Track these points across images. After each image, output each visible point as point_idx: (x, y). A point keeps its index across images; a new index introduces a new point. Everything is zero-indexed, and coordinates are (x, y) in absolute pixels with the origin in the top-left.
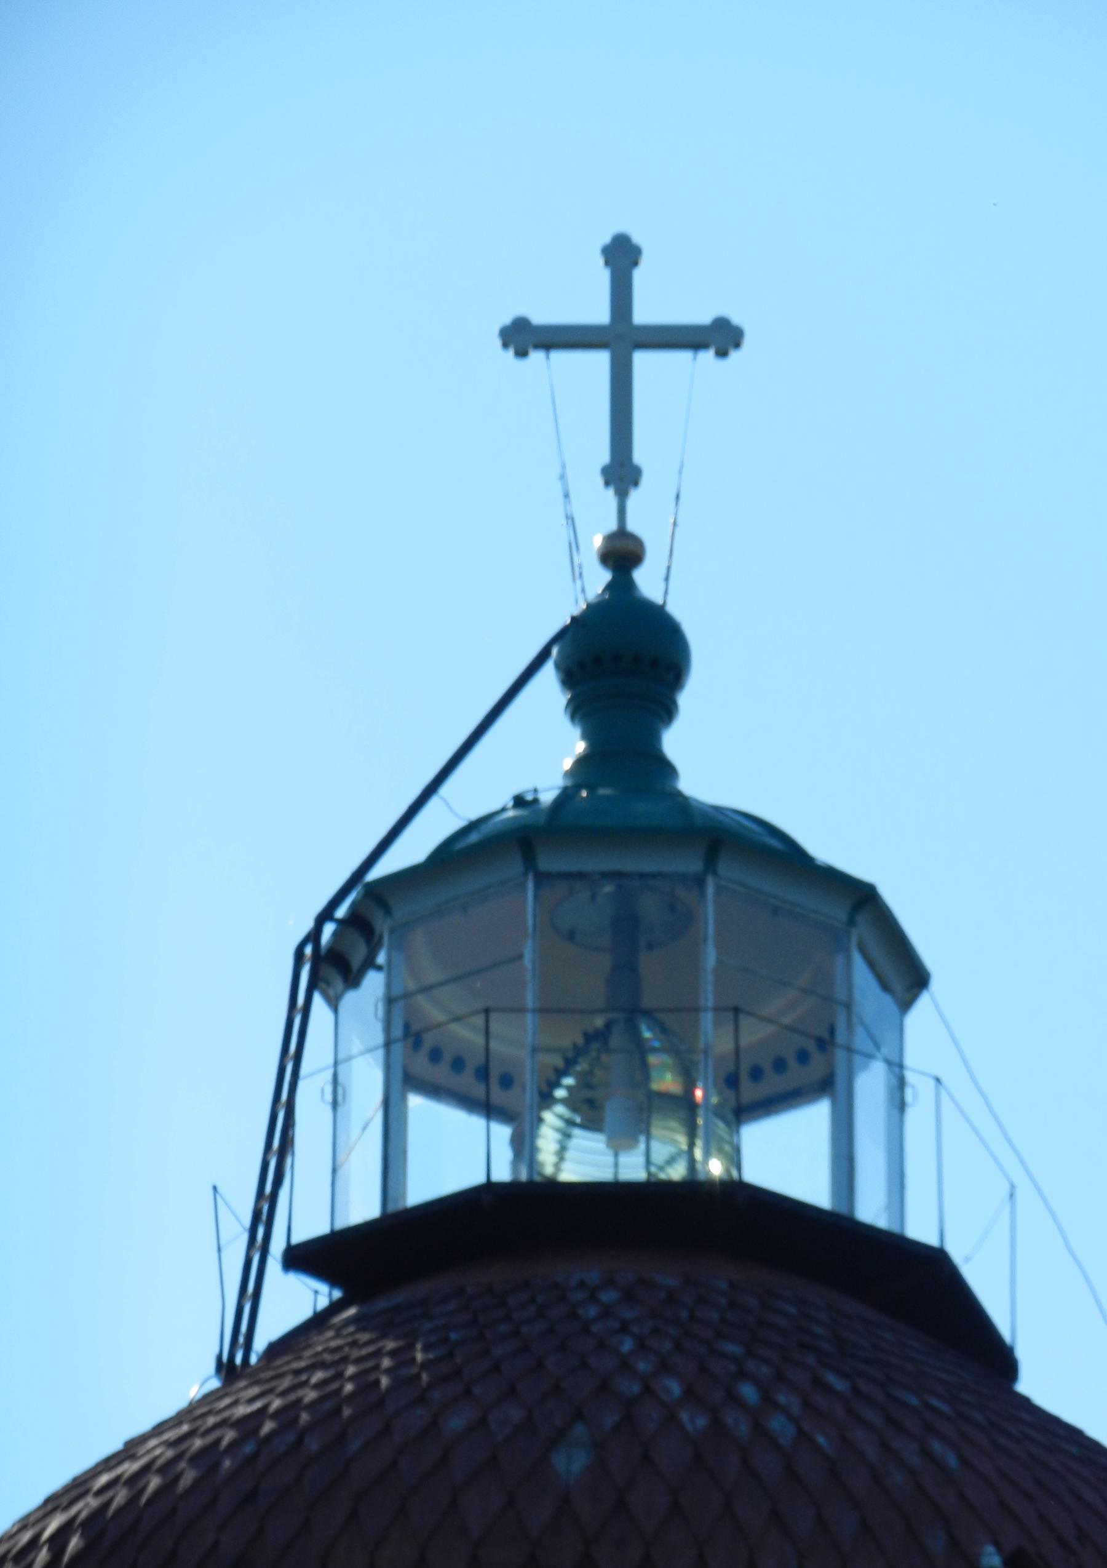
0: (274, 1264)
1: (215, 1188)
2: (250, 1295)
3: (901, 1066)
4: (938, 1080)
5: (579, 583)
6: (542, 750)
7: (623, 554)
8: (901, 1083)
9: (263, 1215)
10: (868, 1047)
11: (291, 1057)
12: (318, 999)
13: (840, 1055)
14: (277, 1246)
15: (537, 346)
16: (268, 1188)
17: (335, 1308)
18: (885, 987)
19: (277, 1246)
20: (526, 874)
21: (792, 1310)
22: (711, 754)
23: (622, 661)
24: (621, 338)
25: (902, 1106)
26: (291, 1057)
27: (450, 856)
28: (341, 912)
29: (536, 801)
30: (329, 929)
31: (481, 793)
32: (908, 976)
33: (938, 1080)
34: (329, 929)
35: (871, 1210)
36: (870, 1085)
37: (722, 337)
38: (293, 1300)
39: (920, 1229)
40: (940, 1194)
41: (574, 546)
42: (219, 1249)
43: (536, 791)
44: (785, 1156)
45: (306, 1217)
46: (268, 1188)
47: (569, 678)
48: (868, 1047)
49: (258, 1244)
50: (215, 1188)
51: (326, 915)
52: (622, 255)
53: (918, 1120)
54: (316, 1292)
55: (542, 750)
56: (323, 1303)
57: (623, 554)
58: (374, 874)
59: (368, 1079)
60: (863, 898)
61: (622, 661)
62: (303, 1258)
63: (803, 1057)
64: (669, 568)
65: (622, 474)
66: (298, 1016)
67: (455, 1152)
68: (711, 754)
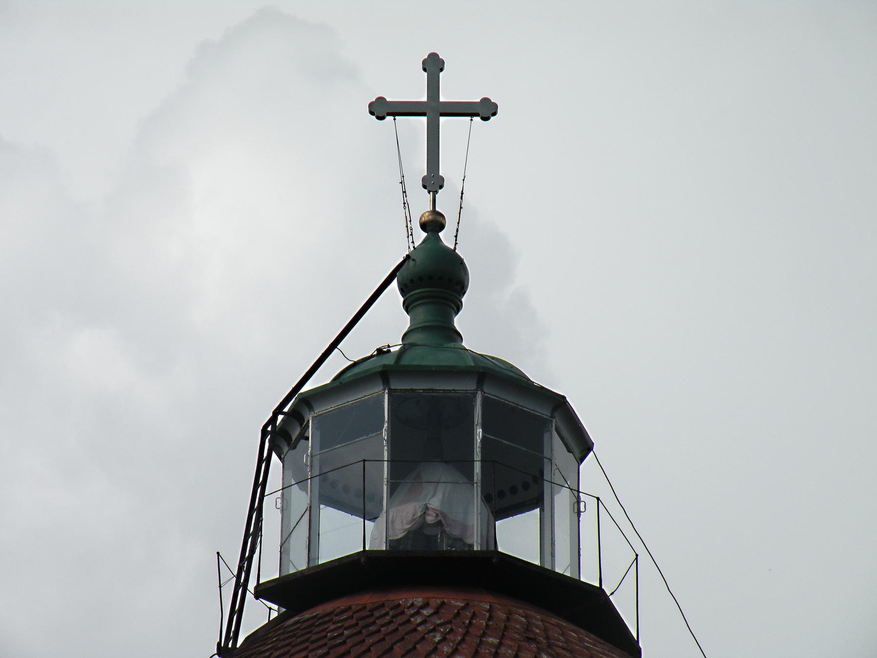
0: (249, 596)
1: (218, 553)
2: (237, 612)
3: (579, 492)
4: (598, 499)
5: (410, 237)
6: (390, 324)
7: (434, 224)
8: (579, 501)
9: (246, 561)
10: (562, 482)
11: (260, 484)
12: (274, 456)
13: (547, 486)
14: (252, 585)
15: (389, 114)
16: (265, 454)
17: (281, 618)
18: (569, 451)
19: (252, 585)
20: (384, 390)
21: (523, 619)
22: (478, 328)
23: (434, 280)
24: (434, 110)
25: (579, 513)
26: (260, 484)
27: (345, 382)
28: (286, 410)
29: (389, 351)
30: (280, 418)
31: (359, 347)
32: (582, 445)
33: (598, 499)
34: (280, 418)
35: (562, 567)
36: (562, 500)
37: (485, 110)
38: (259, 614)
39: (589, 577)
40: (599, 559)
41: (408, 220)
42: (220, 587)
43: (389, 346)
44: (518, 537)
45: (268, 567)
46: (265, 454)
47: (403, 290)
48: (562, 482)
49: (241, 585)
50: (218, 553)
51: (278, 411)
52: (433, 65)
53: (588, 520)
54: (270, 609)
55: (390, 324)
56: (274, 615)
57: (434, 224)
58: (306, 388)
59: (300, 499)
60: (559, 404)
61: (434, 280)
62: (263, 592)
63: (526, 486)
64: (457, 230)
65: (433, 182)
66: (263, 461)
67: (344, 536)
68: (478, 328)
